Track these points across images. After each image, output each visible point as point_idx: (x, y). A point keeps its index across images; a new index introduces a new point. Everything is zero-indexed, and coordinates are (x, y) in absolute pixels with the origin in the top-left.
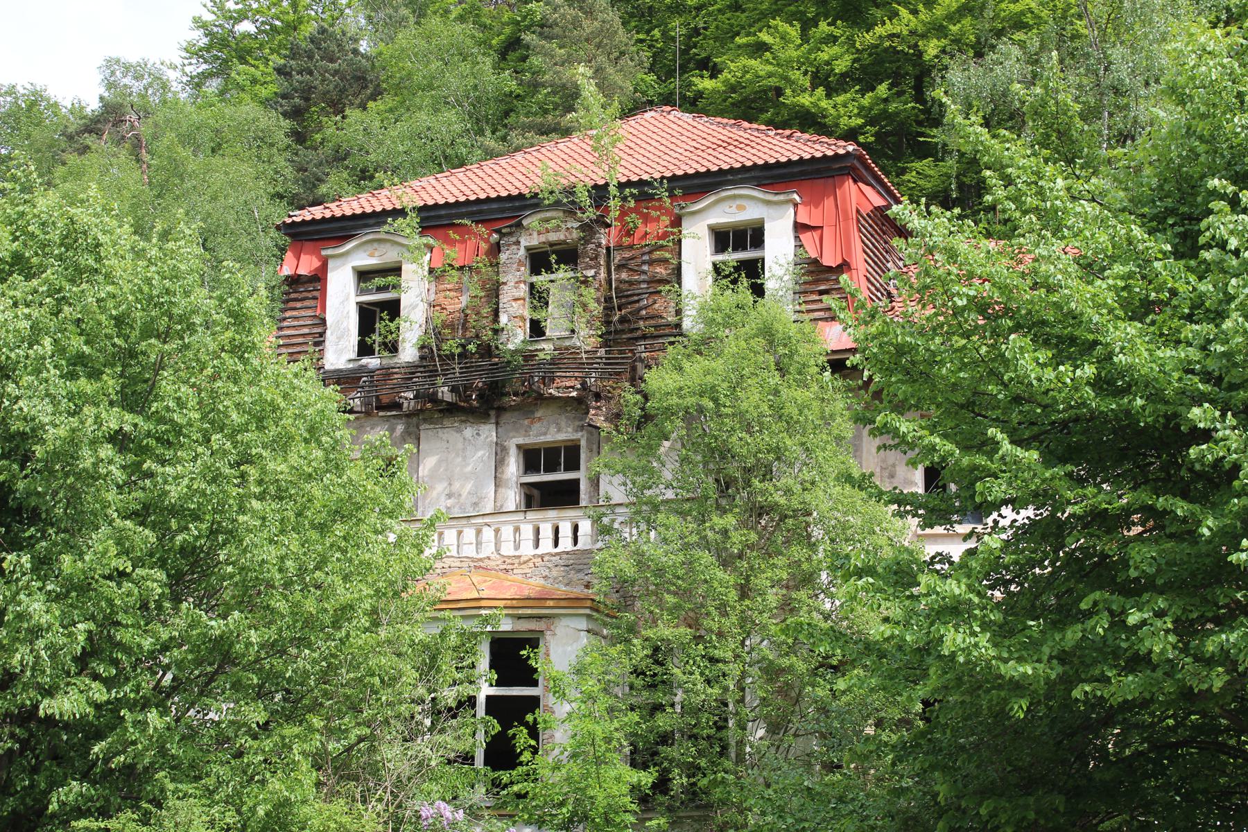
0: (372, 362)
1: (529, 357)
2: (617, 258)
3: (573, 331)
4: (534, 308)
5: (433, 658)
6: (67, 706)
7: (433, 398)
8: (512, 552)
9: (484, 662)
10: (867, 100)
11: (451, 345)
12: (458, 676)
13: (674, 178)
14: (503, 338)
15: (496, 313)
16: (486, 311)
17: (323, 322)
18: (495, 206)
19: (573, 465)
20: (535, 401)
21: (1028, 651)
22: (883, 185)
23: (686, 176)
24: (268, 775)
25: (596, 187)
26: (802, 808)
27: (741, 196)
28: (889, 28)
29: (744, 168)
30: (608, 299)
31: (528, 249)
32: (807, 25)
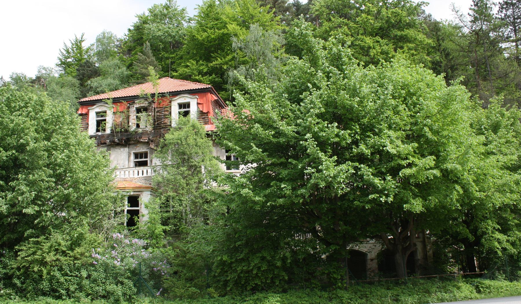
0: (100, 133)
1: (136, 132)
2: (156, 110)
3: (146, 126)
4: (138, 121)
5: (115, 200)
6: (29, 211)
7: (114, 142)
8: (133, 177)
9: (126, 203)
10: (210, 78)
11: (118, 129)
12: (121, 205)
13: (170, 92)
14: (130, 128)
15: (128, 122)
16: (126, 121)
17: (88, 124)
18: (128, 98)
19: (146, 157)
20: (138, 142)
21: (258, 195)
22: (217, 95)
23: (172, 92)
24: (77, 227)
25: (152, 94)
26: (203, 233)
27: (184, 97)
28: (216, 62)
29: (186, 90)
30: (154, 119)
31: (136, 108)
32: (197, 62)
